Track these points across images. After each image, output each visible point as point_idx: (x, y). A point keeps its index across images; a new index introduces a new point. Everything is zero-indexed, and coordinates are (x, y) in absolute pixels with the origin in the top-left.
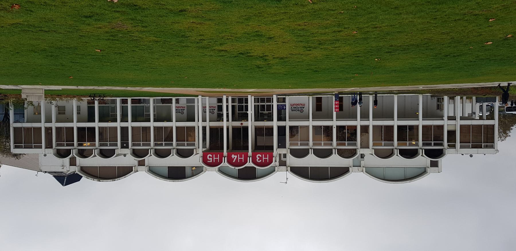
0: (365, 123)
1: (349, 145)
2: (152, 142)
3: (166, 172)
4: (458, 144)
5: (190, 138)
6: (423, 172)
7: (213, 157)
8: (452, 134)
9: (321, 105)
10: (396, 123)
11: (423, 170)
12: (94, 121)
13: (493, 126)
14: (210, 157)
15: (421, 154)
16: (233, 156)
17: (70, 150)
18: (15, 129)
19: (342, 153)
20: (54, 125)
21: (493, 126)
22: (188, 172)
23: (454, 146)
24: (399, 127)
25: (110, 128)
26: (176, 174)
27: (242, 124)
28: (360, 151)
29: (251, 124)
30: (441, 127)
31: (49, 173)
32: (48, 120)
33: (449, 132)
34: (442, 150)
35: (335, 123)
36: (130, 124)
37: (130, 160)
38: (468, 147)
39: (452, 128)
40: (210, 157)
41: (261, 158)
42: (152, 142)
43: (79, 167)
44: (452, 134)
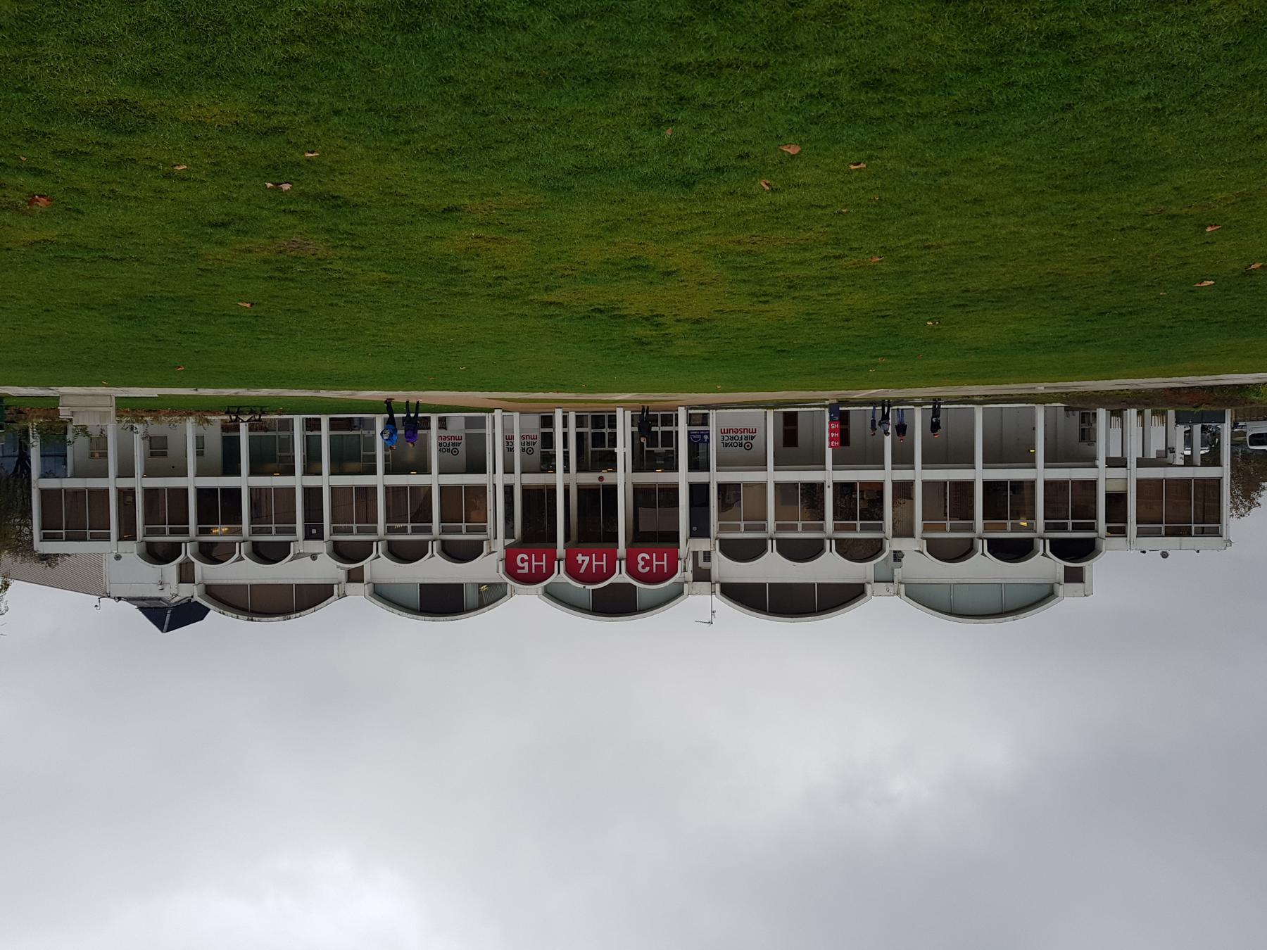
0: (903, 475)
1: (864, 528)
2: (381, 525)
3: (415, 598)
4: (1132, 526)
5: (473, 514)
6: (1046, 595)
7: (530, 561)
8: (1116, 501)
9: (795, 432)
10: (979, 474)
11: (1047, 591)
12: (238, 474)
13: (1218, 482)
14: (523, 560)
15: (1041, 551)
16: (580, 558)
17: (371, 543)
18: (44, 493)
19: (849, 550)
20: (139, 483)
21: (1218, 482)
22: (470, 597)
23: (1122, 532)
24: (987, 485)
25: (278, 490)
26: (441, 602)
27: (601, 478)
28: (892, 545)
29: (623, 478)
30: (1093, 484)
31: (129, 600)
32: (126, 470)
33: (1109, 496)
34: (1093, 540)
35: (829, 476)
36: (326, 481)
37: (325, 569)
38: (1157, 533)
39: (1117, 488)
40: (523, 560)
41: (648, 563)
42: (381, 525)
43: (202, 587)
44: (1116, 501)
